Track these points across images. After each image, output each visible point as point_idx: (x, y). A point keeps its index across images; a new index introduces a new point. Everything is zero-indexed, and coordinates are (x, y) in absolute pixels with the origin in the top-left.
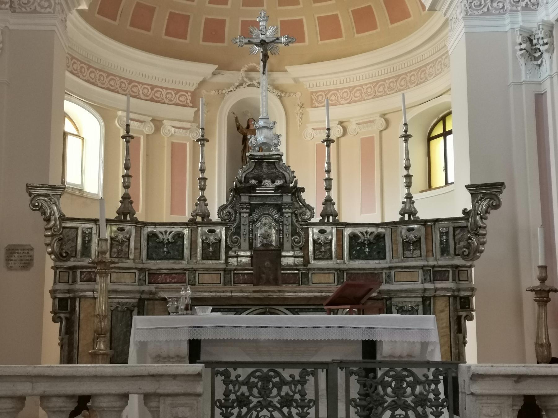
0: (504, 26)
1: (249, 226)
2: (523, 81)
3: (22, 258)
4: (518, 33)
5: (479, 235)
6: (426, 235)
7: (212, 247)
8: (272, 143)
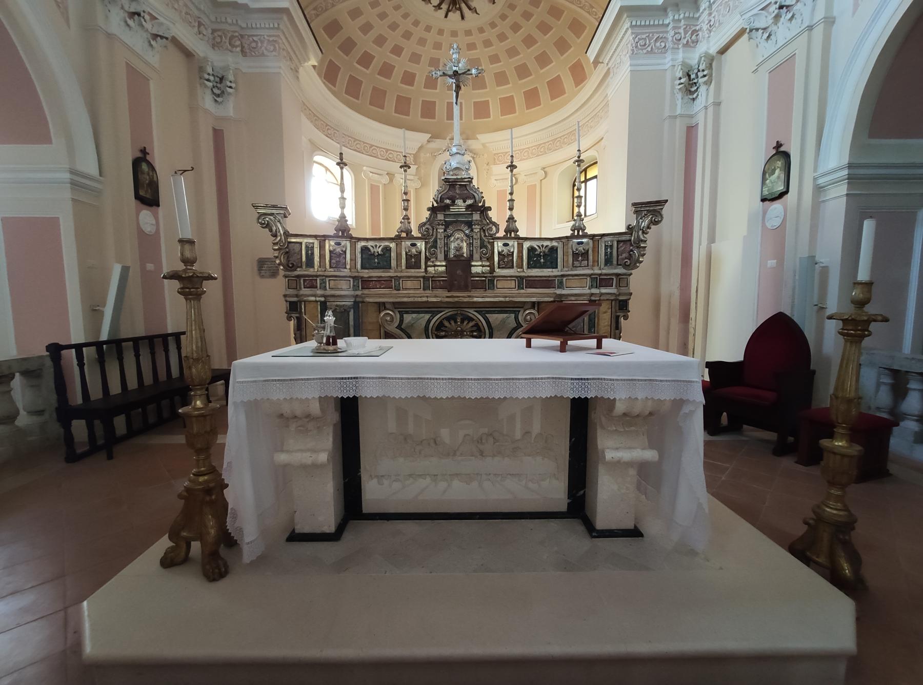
0: (664, 64)
1: (444, 240)
2: (679, 114)
3: (270, 269)
4: (680, 67)
5: (640, 248)
6: (594, 247)
7: (414, 258)
8: (463, 168)
